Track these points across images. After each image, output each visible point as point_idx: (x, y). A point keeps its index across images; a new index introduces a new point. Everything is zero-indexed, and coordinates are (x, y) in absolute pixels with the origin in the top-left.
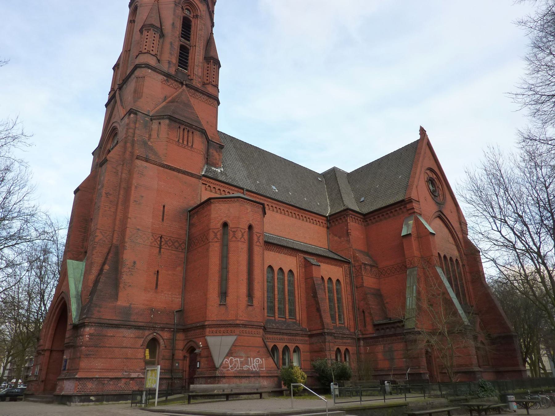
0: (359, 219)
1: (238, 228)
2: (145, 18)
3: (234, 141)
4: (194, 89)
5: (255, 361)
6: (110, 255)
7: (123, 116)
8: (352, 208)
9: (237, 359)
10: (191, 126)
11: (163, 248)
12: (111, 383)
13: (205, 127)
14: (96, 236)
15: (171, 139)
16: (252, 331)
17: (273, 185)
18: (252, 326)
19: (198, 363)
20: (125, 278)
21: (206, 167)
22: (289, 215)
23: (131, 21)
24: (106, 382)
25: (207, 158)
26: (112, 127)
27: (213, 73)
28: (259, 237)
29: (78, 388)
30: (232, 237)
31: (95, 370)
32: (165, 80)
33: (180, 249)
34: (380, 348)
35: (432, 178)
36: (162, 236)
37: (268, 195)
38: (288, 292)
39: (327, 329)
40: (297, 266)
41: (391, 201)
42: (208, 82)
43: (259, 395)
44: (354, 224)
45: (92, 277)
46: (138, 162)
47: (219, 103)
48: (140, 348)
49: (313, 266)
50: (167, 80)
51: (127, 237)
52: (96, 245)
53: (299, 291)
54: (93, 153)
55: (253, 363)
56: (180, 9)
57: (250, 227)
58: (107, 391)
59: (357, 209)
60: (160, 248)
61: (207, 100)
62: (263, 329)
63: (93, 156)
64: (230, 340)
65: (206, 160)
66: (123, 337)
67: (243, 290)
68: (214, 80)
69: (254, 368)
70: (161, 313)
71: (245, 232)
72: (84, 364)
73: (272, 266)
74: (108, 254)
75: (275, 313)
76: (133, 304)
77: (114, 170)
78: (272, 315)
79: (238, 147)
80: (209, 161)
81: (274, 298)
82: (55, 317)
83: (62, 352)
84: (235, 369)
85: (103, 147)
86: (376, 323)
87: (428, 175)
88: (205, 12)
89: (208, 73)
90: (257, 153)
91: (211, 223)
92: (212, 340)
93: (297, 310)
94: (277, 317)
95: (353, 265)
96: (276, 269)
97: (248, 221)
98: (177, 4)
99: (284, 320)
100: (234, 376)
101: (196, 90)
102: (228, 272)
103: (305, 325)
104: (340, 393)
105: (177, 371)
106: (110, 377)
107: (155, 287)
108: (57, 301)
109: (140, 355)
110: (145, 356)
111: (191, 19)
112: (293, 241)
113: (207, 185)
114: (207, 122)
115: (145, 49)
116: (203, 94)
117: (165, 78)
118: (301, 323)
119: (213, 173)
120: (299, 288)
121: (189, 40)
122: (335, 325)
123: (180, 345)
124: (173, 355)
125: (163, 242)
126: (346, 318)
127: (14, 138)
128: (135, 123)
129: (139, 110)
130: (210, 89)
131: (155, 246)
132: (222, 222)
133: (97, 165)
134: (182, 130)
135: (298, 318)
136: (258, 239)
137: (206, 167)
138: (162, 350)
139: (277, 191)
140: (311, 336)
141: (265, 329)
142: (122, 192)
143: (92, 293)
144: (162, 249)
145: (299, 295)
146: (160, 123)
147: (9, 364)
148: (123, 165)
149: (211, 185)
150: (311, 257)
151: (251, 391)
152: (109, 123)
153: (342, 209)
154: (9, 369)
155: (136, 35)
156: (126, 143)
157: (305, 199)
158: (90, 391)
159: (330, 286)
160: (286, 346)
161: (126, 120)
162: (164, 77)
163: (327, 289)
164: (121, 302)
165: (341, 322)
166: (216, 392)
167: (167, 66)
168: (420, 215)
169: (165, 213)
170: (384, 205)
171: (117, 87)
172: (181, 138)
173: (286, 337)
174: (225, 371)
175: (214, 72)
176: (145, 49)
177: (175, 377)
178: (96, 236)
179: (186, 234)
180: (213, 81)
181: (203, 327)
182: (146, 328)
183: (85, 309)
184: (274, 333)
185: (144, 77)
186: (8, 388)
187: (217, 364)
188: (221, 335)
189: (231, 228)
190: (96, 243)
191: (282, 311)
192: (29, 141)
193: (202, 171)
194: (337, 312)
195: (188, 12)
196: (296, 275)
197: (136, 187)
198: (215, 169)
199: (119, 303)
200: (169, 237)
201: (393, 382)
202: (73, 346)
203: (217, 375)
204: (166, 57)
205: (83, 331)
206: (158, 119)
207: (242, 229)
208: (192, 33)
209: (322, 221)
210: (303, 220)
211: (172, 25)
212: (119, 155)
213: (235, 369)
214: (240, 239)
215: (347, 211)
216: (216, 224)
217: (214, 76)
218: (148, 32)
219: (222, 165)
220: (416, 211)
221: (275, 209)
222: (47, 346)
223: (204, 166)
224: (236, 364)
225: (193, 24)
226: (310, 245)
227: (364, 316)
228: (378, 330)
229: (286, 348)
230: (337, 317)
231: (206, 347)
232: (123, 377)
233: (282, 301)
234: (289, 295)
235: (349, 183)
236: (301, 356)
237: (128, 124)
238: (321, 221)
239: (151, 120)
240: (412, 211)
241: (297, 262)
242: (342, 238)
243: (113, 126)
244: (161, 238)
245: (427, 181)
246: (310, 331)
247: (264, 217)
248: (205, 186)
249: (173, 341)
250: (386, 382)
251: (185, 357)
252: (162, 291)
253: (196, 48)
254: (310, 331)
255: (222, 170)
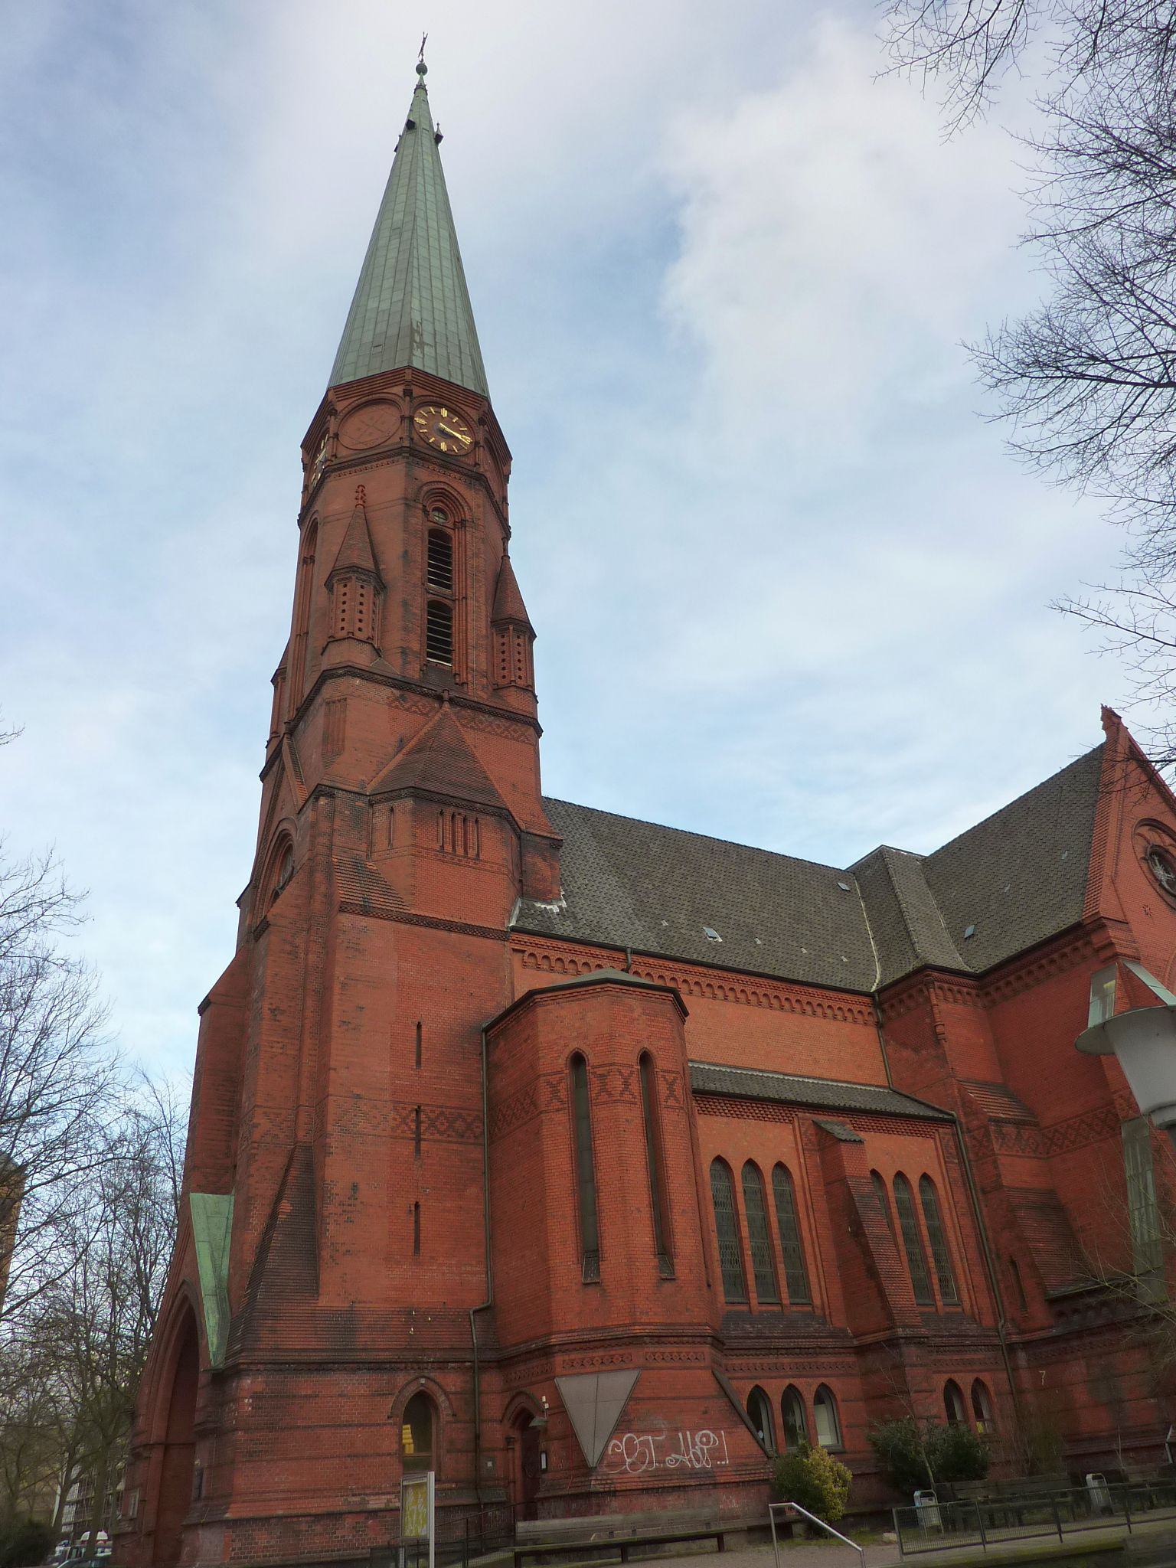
0: (965, 990)
1: (611, 1064)
2: (335, 549)
3: (592, 819)
4: (473, 708)
5: (697, 1440)
6: (293, 1173)
7: (301, 804)
8: (942, 961)
9: (646, 1437)
10: (470, 805)
11: (425, 1140)
12: (318, 1528)
13: (510, 800)
14: (255, 1126)
15: (422, 848)
16: (679, 1353)
17: (709, 926)
18: (678, 1338)
19: (544, 1457)
20: (334, 1231)
21: (519, 904)
22: (760, 1004)
23: (306, 560)
24: (304, 1527)
25: (521, 881)
26: (277, 833)
27: (517, 657)
28: (672, 1084)
29: (233, 1550)
30: (598, 1094)
31: (276, 1496)
32: (397, 699)
33: (469, 1138)
34: (1077, 1370)
35: (1159, 846)
36: (419, 1107)
37: (695, 957)
38: (780, 1228)
39: (905, 1326)
40: (797, 1150)
41: (1048, 930)
42: (505, 682)
43: (716, 1539)
44: (951, 1006)
45: (253, 1236)
46: (345, 920)
47: (539, 732)
48: (385, 1424)
49: (843, 1145)
50: (402, 696)
51: (331, 1118)
52: (257, 1149)
53: (812, 1221)
54: (239, 903)
55: (693, 1447)
56: (420, 513)
57: (645, 1058)
58: (309, 1552)
59: (957, 961)
60: (418, 1140)
61: (507, 729)
62: (712, 1345)
63: (239, 910)
64: (621, 1382)
65: (518, 885)
66: (340, 1396)
67: (644, 1238)
68: (522, 673)
69: (698, 1461)
70: (434, 1320)
71: (632, 1073)
72: (243, 1480)
73: (724, 1156)
74: (287, 1171)
75: (748, 1292)
76: (359, 1303)
77: (288, 948)
78: (740, 1300)
79: (605, 834)
80: (526, 888)
81: (742, 1249)
82: (170, 1350)
83: (190, 1446)
84: (644, 1467)
85: (261, 885)
86: (1054, 1293)
87: (1145, 838)
88: (481, 509)
89: (503, 660)
90: (658, 842)
91: (539, 1059)
92: (575, 1389)
93: (813, 1278)
94: (754, 1302)
95: (964, 1126)
96: (737, 1165)
97: (638, 1042)
98: (412, 503)
99: (776, 1309)
100: (643, 1489)
101: (477, 707)
102: (596, 1190)
103: (839, 1321)
104: (945, 1519)
105: (491, 1483)
106: (313, 1511)
107: (412, 1250)
108: (172, 1306)
109: (388, 1445)
110: (402, 1447)
111: (450, 532)
112: (781, 1077)
113: (527, 954)
114: (514, 785)
115: (343, 629)
116: (496, 715)
117: (397, 693)
118: (827, 1313)
119: (540, 918)
120: (811, 1213)
121: (449, 587)
122: (934, 1309)
123: (494, 1405)
124: (477, 1437)
125: (423, 1122)
126: (964, 1286)
127: (47, 905)
128: (332, 819)
129: (338, 785)
130: (514, 701)
131: (405, 1135)
132: (567, 1052)
133: (250, 932)
134: (448, 818)
135: (817, 1302)
136: (671, 1090)
137: (519, 904)
138: (446, 1422)
139: (720, 940)
140: (861, 1351)
141: (717, 1342)
142: (309, 1003)
143: (255, 1280)
144: (422, 1142)
145: (814, 1233)
146: (392, 810)
147: (76, 1487)
148: (309, 930)
149: (536, 951)
150: (835, 1119)
151: (692, 1532)
152: (268, 831)
153: (911, 969)
154: (78, 1502)
155: (320, 597)
156: (312, 872)
157: (805, 951)
158: (265, 1556)
159: (905, 1196)
160: (791, 1386)
161: (309, 814)
162: (395, 691)
163: (894, 1205)
164: (329, 1300)
165: (950, 1301)
166: (593, 1539)
167: (400, 661)
168: (1136, 959)
169: (424, 1045)
170: (1029, 943)
171: (283, 729)
172: (448, 840)
173: (786, 1360)
174: (615, 1477)
175: (519, 653)
176: (343, 629)
177: (486, 1501)
178: (255, 1126)
179: (483, 1094)
180: (520, 677)
181: (547, 1351)
182: (398, 1365)
183: (238, 1326)
184: (751, 1352)
185: (345, 700)
186: (74, 1559)
187: (592, 1459)
188: (595, 1372)
189: (593, 1067)
190: (256, 1145)
191: (769, 1285)
192: (77, 912)
193: (510, 916)
194: (934, 1270)
195: (441, 515)
196: (798, 1172)
197: (344, 985)
198: (543, 906)
199: (323, 1302)
200: (438, 1107)
201: (1113, 1477)
202: (215, 1432)
203: (592, 1489)
204: (395, 639)
205: (237, 1387)
206: (388, 800)
207: (623, 1065)
208: (455, 567)
209: (859, 1008)
210: (804, 1012)
211: (404, 557)
212: (297, 906)
213: (644, 1467)
214: (622, 1094)
215: (925, 972)
216: (554, 1061)
217: (520, 665)
218: (345, 586)
219: (563, 893)
220: (1119, 949)
221: (719, 993)
222: (156, 1434)
223: (514, 903)
224: (643, 1454)
225: (455, 544)
226: (832, 1080)
227: (1017, 1275)
228: (1061, 1314)
229: (791, 1395)
230: (936, 1287)
231: (560, 1408)
232: (345, 1508)
233: (765, 1255)
234: (783, 1237)
235: (929, 886)
236: (838, 1413)
237: (314, 825)
238: (856, 1008)
239: (371, 805)
240: (1108, 953)
241: (795, 1136)
242: (924, 1052)
243: (280, 829)
244: (418, 1111)
245: (1144, 858)
246: (856, 1336)
247: (684, 1022)
248: (520, 955)
249: (472, 1396)
250: (1089, 1477)
251: (509, 1440)
252: (432, 1258)
253: (468, 601)
254: (856, 1336)
255: (564, 904)
